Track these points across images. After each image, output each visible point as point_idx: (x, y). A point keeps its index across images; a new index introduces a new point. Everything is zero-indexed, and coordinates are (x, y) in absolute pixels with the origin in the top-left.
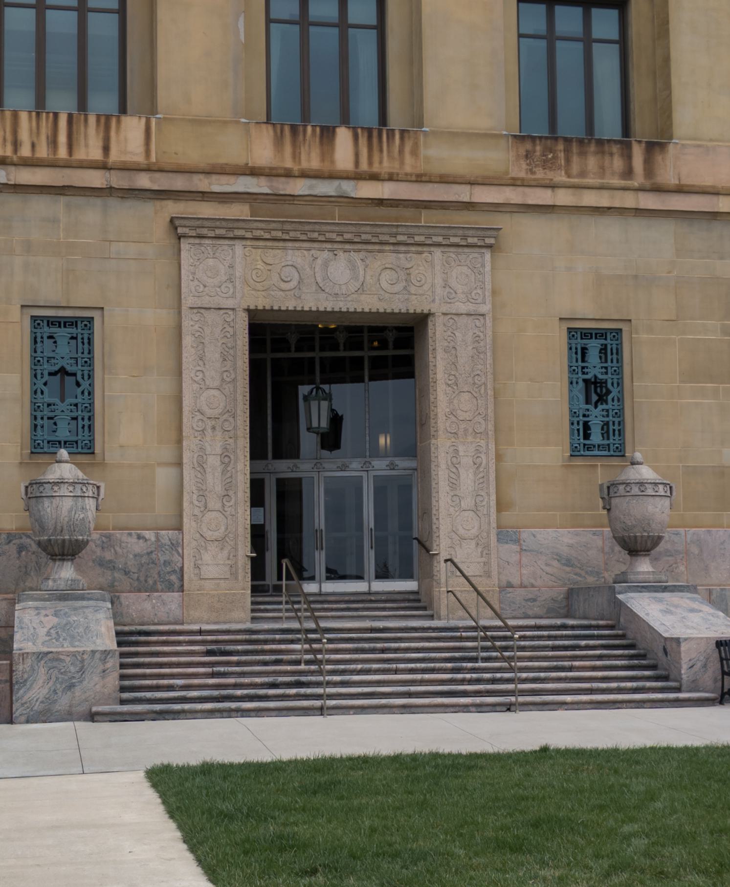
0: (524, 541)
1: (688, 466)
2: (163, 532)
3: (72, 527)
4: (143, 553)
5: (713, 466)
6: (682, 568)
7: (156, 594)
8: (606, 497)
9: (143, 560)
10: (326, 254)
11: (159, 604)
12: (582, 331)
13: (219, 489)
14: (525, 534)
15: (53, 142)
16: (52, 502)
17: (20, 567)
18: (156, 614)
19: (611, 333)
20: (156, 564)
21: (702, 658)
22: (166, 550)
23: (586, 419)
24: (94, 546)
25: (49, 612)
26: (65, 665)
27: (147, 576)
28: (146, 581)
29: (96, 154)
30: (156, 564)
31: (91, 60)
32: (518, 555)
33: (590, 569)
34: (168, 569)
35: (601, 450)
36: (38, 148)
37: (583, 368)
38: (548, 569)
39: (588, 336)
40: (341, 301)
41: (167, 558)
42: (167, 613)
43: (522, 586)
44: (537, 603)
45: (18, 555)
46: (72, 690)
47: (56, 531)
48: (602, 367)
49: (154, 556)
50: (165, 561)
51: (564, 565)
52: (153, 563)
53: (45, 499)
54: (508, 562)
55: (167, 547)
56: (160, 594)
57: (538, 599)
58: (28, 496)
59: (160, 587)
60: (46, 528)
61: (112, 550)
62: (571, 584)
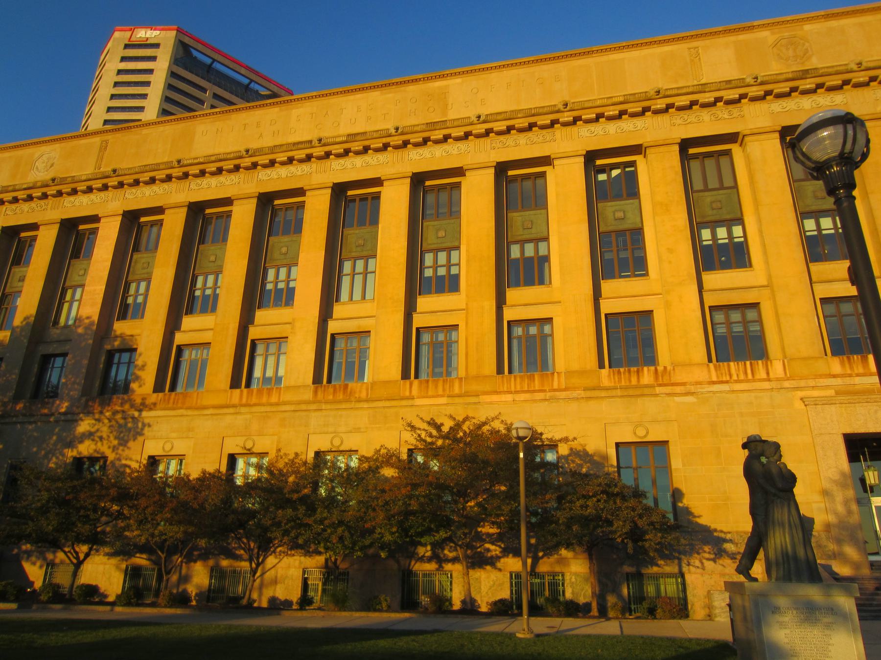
15: (746, 373)
29: (764, 376)
31: (730, 171)
36: (739, 376)
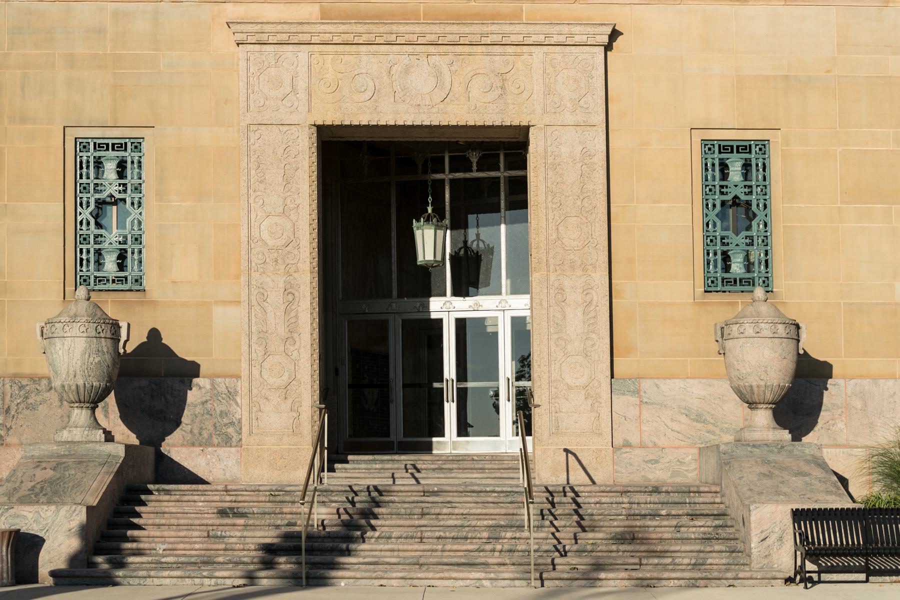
0: (645, 392)
1: (851, 304)
2: (220, 380)
3: (86, 372)
4: (196, 402)
5: (882, 304)
6: (841, 425)
7: (210, 449)
8: (720, 340)
9: (197, 410)
10: (405, 60)
11: (214, 460)
12: (720, 143)
13: (282, 330)
14: (646, 385)
16: (63, 344)
17: (62, 417)
18: (210, 471)
19: (756, 145)
20: (211, 415)
21: (777, 530)
22: (223, 399)
23: (725, 248)
24: (143, 395)
25: (653, 480)
26: (27, 522)
27: (201, 428)
28: (200, 434)
30: (211, 415)
32: (638, 408)
33: (727, 426)
34: (225, 421)
35: (744, 285)
37: (722, 187)
38: (675, 426)
39: (728, 149)
40: (424, 113)
41: (223, 408)
42: (224, 470)
43: (642, 446)
44: (660, 466)
45: (60, 404)
46: (35, 550)
47: (69, 376)
48: (745, 186)
49: (209, 406)
50: (221, 412)
51: (694, 420)
52: (208, 413)
53: (57, 340)
54: (625, 417)
55: (224, 396)
56: (215, 449)
57: (661, 460)
58: (44, 337)
59: (216, 441)
60: (59, 372)
61: (163, 400)
62: (702, 443)
